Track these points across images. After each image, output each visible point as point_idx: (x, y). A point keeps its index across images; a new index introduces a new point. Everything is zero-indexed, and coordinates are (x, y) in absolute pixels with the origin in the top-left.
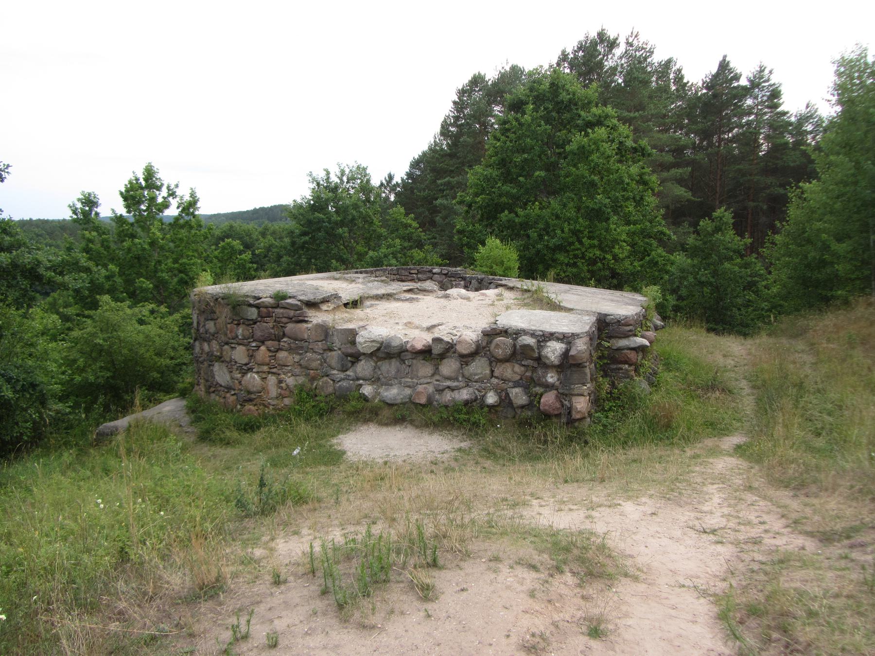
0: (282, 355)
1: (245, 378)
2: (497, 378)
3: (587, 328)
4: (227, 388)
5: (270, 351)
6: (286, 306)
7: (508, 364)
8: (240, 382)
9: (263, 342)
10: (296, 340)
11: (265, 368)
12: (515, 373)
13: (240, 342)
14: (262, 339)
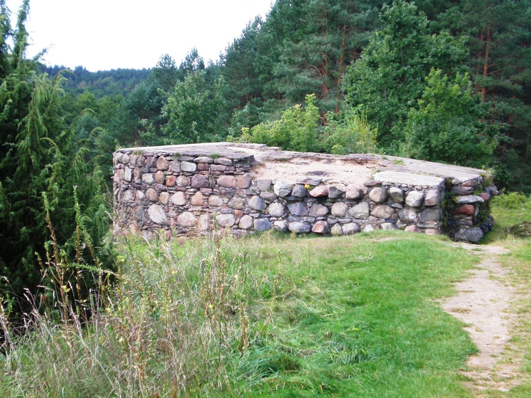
0: (213, 198)
1: (180, 216)
2: (373, 216)
3: (438, 184)
4: (162, 225)
5: (204, 195)
6: (220, 162)
7: (382, 206)
8: (176, 219)
9: (199, 189)
10: (225, 187)
11: (199, 208)
12: (387, 212)
13: (179, 188)
14: (198, 186)
